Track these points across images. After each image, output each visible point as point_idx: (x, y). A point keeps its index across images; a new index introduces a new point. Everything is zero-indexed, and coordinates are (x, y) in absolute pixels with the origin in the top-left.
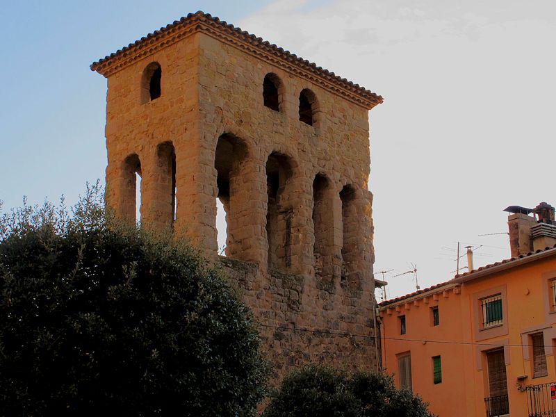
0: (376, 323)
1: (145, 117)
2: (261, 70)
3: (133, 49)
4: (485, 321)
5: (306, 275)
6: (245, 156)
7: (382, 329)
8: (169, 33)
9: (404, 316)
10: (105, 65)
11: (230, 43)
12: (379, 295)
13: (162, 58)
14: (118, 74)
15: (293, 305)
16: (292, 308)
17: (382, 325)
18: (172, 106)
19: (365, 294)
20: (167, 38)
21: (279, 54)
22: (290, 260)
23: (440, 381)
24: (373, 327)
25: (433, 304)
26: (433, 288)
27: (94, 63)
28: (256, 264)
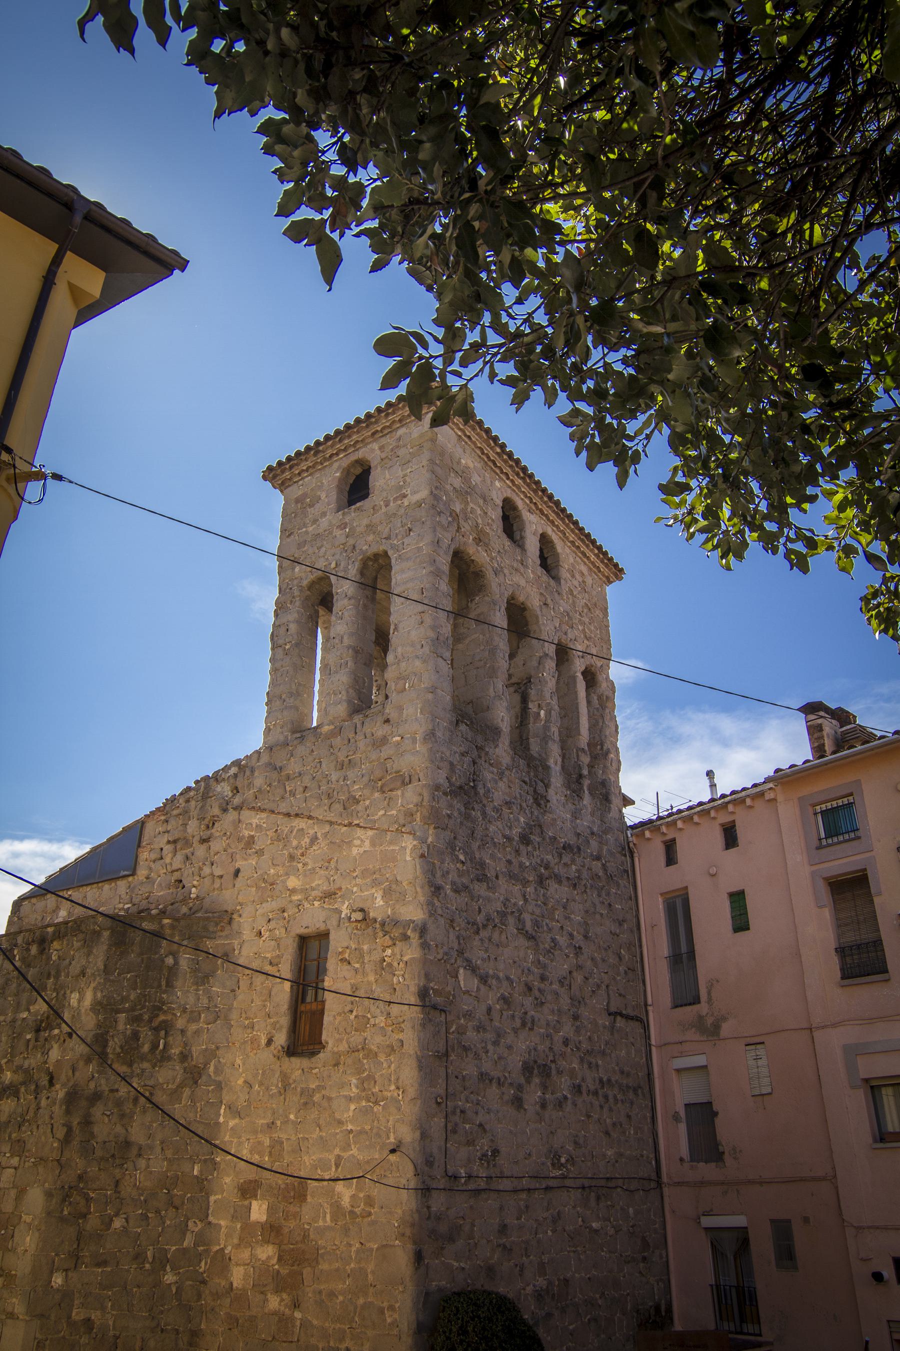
0: (628, 851)
1: (342, 526)
2: (499, 489)
3: (330, 443)
4: (823, 835)
5: (551, 762)
6: (480, 591)
7: (636, 860)
8: (387, 415)
9: (674, 840)
10: (285, 469)
11: (467, 440)
12: (632, 815)
13: (372, 452)
14: (301, 482)
15: (540, 800)
16: (539, 805)
17: (636, 855)
18: (386, 506)
19: (613, 814)
20: (384, 422)
21: (522, 475)
22: (528, 744)
23: (747, 928)
24: (625, 856)
25: (724, 818)
26: (733, 793)
27: (270, 468)
28: (496, 732)
